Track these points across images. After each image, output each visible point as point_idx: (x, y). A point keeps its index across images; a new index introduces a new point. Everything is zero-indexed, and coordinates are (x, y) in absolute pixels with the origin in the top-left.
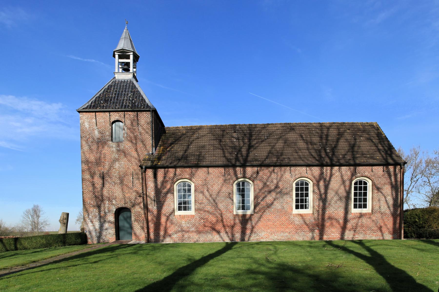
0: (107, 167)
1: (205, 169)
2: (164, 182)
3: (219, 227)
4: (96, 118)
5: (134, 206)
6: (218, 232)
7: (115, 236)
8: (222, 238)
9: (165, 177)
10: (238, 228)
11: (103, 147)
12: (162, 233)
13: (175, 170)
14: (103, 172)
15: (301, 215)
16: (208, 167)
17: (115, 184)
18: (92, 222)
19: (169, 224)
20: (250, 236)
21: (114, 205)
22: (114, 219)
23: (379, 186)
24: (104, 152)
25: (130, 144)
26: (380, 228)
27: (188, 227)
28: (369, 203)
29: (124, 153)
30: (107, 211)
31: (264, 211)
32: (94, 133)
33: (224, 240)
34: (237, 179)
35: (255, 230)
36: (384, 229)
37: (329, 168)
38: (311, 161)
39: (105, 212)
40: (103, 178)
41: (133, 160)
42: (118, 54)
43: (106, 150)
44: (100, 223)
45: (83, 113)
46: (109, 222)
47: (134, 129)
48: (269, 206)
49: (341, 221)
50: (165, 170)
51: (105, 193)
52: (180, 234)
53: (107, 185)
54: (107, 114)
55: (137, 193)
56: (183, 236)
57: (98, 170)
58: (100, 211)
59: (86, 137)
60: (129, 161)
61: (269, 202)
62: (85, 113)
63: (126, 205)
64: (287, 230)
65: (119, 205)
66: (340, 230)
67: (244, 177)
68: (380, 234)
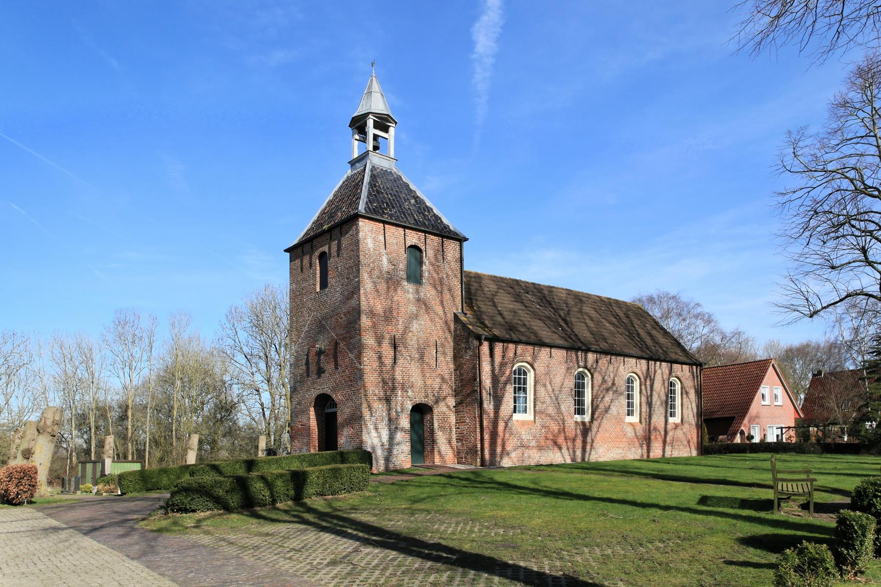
0: (400, 327)
1: (548, 349)
2: (503, 365)
3: (561, 440)
4: (385, 235)
5: (437, 402)
6: (560, 448)
8: (563, 457)
9: (503, 357)
10: (579, 443)
11: (395, 290)
12: (499, 450)
14: (394, 336)
15: (631, 424)
16: (551, 346)
17: (411, 360)
18: (376, 429)
19: (507, 436)
20: (590, 455)
21: (410, 398)
22: (409, 426)
23: (687, 389)
24: (395, 298)
25: (433, 292)
26: (689, 442)
27: (528, 440)
28: (678, 410)
29: (425, 305)
30: (399, 410)
31: (602, 418)
32: (381, 261)
33: (565, 461)
34: (579, 367)
35: (594, 445)
36: (691, 444)
37: (653, 362)
38: (639, 353)
39: (396, 412)
40: (395, 347)
41: (437, 320)
42: (374, 120)
43: (399, 296)
44: (388, 432)
45: (365, 220)
46: (402, 430)
47: (439, 267)
48: (607, 410)
49: (663, 433)
50: (503, 346)
51: (398, 377)
52: (519, 451)
53: (400, 361)
54: (401, 230)
55: (443, 379)
56: (523, 454)
57: (389, 331)
58: (389, 410)
59: (368, 265)
60: (432, 320)
61: (607, 405)
62: (368, 221)
63: (426, 399)
64: (621, 446)
66: (662, 445)
67: (585, 367)
68: (689, 449)
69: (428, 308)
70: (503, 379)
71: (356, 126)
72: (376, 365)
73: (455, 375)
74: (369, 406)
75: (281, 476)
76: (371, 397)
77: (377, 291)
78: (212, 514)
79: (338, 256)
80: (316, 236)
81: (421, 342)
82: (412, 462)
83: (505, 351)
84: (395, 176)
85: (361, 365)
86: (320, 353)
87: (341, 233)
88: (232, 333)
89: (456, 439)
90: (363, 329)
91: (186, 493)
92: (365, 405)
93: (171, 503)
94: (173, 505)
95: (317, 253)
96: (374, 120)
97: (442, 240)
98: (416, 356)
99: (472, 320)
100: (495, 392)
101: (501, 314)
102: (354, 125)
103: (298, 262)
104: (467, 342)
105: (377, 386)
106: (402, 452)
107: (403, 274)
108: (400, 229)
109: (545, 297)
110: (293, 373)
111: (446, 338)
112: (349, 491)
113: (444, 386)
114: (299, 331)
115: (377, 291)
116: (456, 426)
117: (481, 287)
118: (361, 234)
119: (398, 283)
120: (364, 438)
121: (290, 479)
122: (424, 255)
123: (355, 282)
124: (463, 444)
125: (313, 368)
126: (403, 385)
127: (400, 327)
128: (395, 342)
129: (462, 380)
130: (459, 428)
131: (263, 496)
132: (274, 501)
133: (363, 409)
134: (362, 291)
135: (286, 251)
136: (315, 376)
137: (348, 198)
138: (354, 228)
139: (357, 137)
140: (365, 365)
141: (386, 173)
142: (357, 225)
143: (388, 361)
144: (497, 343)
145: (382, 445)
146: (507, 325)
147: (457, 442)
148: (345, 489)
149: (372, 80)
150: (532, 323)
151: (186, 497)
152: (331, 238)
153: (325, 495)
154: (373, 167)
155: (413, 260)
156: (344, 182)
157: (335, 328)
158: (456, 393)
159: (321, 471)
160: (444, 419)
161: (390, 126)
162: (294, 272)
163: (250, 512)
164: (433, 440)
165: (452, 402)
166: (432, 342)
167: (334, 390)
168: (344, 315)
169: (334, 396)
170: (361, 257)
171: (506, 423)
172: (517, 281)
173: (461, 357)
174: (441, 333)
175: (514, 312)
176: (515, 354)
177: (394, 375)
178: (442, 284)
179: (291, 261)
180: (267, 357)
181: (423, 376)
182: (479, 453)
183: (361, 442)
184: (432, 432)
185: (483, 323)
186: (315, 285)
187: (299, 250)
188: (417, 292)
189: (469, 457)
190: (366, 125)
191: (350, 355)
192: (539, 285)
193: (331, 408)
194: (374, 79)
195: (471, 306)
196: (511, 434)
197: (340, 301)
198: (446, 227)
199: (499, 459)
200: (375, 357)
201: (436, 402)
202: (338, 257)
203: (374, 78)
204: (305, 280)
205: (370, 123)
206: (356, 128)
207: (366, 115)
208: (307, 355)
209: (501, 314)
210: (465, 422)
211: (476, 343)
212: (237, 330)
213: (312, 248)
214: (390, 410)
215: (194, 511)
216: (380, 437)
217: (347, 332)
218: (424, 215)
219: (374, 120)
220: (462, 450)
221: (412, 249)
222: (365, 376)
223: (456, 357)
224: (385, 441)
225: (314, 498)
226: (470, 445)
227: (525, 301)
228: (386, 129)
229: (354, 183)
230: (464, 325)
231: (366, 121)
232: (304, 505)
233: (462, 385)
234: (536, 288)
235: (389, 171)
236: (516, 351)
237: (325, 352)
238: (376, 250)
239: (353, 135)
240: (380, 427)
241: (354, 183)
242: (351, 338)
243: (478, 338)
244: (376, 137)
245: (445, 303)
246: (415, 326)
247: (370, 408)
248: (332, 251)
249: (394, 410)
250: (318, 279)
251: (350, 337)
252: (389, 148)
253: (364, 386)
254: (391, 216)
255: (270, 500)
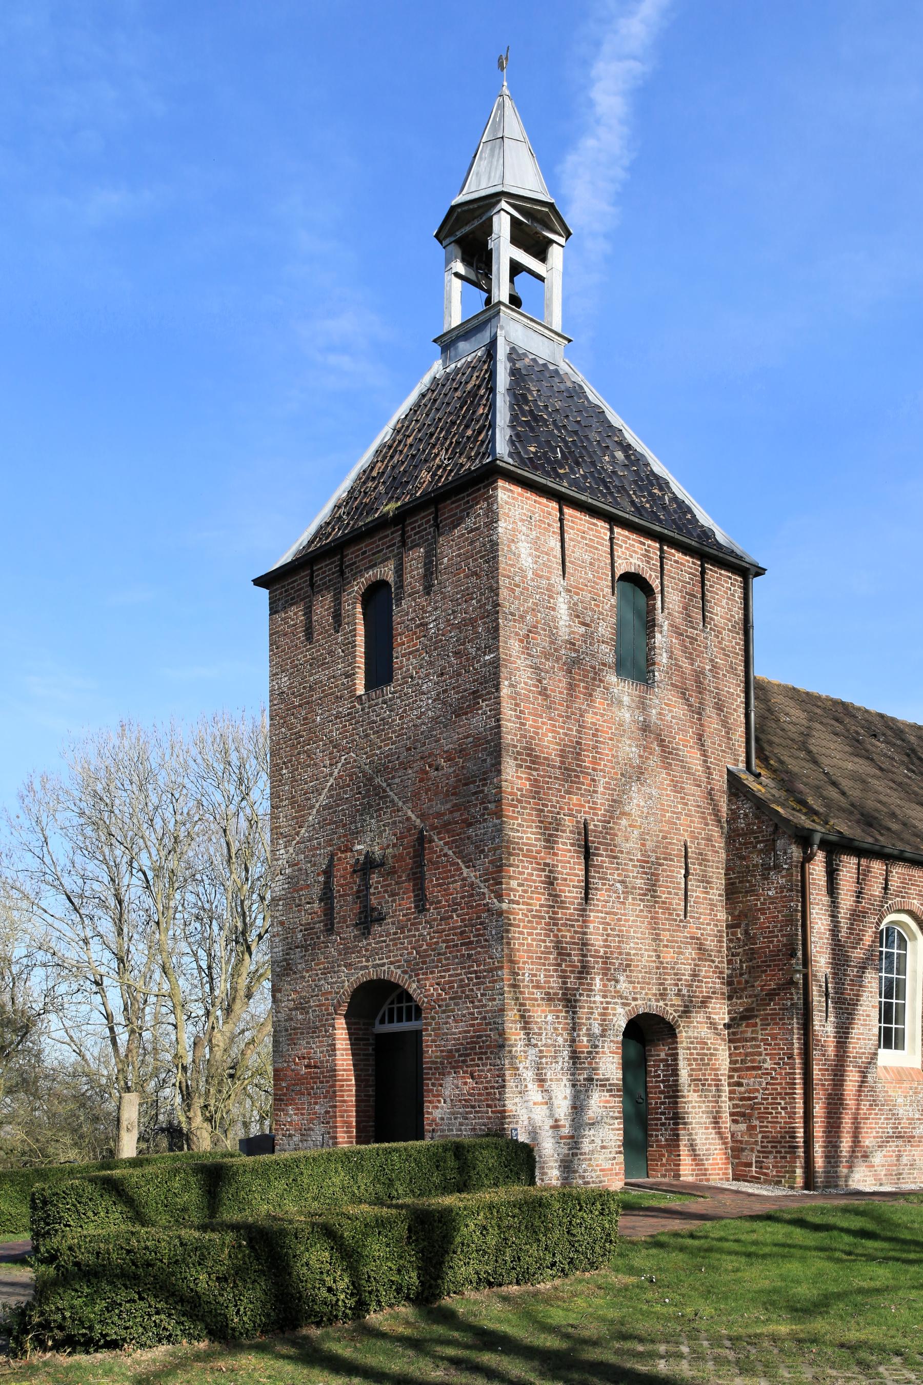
0: (601, 799)
2: (857, 916)
5: (686, 1012)
7: (621, 1158)
9: (859, 894)
12: (846, 1144)
13: (887, 871)
19: (864, 1108)
24: (589, 718)
30: (597, 1030)
40: (588, 854)
41: (690, 788)
42: (512, 217)
45: (512, 487)
46: (604, 1084)
47: (693, 639)
50: (859, 864)
51: (596, 941)
52: (892, 1146)
53: (600, 896)
54: (602, 526)
55: (701, 948)
59: (521, 617)
60: (677, 788)
63: (661, 1003)
65: (639, 1002)
69: (668, 753)
70: (857, 954)
71: (459, 234)
72: (539, 900)
73: (730, 941)
74: (523, 1017)
75: (381, 1224)
76: (528, 992)
77: (544, 693)
78: (173, 1354)
79: (428, 589)
80: (356, 538)
81: (650, 845)
82: (628, 1172)
83: (862, 878)
84: (569, 384)
85: (501, 901)
86: (368, 866)
87: (437, 526)
88: (35, 841)
89: (732, 1114)
90: (507, 799)
91: (89, 1284)
92: (512, 1014)
93: (36, 1320)
94: (45, 1325)
95: (358, 587)
96: (512, 217)
97: (702, 566)
98: (639, 882)
99: (774, 791)
100: (839, 991)
101: (834, 784)
102: (451, 233)
103: (296, 614)
104: (771, 847)
105: (541, 960)
106: (603, 1147)
107: (607, 652)
108: (601, 523)
109: (913, 751)
110: (282, 923)
111: (709, 839)
112: (563, 1271)
113: (705, 970)
114: (300, 807)
115: (544, 693)
116: (730, 1077)
117: (769, 710)
118: (503, 526)
119: (595, 677)
120: (510, 1105)
121: (405, 1234)
122: (659, 604)
123: (485, 665)
124: (751, 1128)
125: (346, 908)
126: (606, 959)
127: (600, 799)
128: (586, 840)
129: (751, 955)
130: (739, 1084)
131: (330, 1290)
132: (361, 1307)
133: (508, 1025)
134: (505, 691)
135: (259, 582)
136: (350, 932)
137: (448, 432)
138: (480, 508)
139: (459, 267)
140: (513, 902)
141: (547, 373)
142: (491, 500)
143: (571, 893)
144: (845, 858)
145: (556, 1127)
146: (856, 812)
147: (735, 1121)
148: (553, 1264)
149: (502, 106)
150: (909, 812)
151: (91, 1300)
152: (403, 543)
153: (500, 1285)
154: (513, 350)
155: (629, 616)
156: (423, 395)
157: (416, 794)
158: (734, 988)
159: (491, 1207)
160: (704, 1060)
161: (552, 242)
162: (283, 641)
163: (294, 1343)
164: (676, 1114)
165: (721, 1012)
166: (677, 849)
167: (413, 969)
168: (449, 759)
169: (412, 988)
170: (504, 593)
171: (864, 1075)
172: (843, 704)
173: (752, 891)
174: (697, 824)
175: (856, 777)
176: (886, 888)
177: (585, 933)
178: (700, 689)
179: (273, 611)
180: (120, 902)
181: (654, 940)
182: (801, 1152)
183: (502, 1115)
184: (673, 1092)
185: (803, 803)
186: (350, 676)
187: (301, 580)
188: (643, 706)
189: (770, 1162)
190: (489, 231)
191: (465, 871)
192: (893, 719)
193: (391, 1021)
194: (508, 103)
195: (763, 758)
196: (874, 1103)
197: (434, 719)
198: (706, 535)
199: (845, 1171)
200: (538, 878)
201: (684, 1012)
202: (428, 594)
203: (507, 99)
204: (318, 663)
205: (502, 225)
206: (459, 242)
207: (489, 202)
208: (328, 873)
209: (834, 784)
210: (759, 1068)
211: (796, 852)
212: (47, 833)
213: (342, 573)
214: (574, 1029)
215: (113, 1345)
216: (549, 1103)
217: (456, 808)
218: (651, 495)
219: (514, 220)
220: (747, 1142)
221: (628, 586)
222: (514, 933)
223: (732, 892)
224: (562, 1117)
225: (470, 1293)
226: (774, 1131)
227: (875, 757)
228: (540, 250)
229: (458, 394)
230: (760, 805)
231: (490, 219)
232: (448, 1317)
233: (751, 969)
234: (888, 727)
235: (552, 367)
236: (886, 880)
237: (382, 864)
238: (541, 577)
239: (448, 261)
240: (548, 1077)
241: (458, 394)
242: (470, 825)
243: (804, 839)
244: (516, 268)
245: (708, 743)
246: (636, 802)
247: (525, 1022)
248: (408, 578)
249: (584, 1031)
250: (361, 661)
251: (464, 821)
252: (550, 306)
253: (512, 962)
254: (574, 483)
255: (351, 1302)
